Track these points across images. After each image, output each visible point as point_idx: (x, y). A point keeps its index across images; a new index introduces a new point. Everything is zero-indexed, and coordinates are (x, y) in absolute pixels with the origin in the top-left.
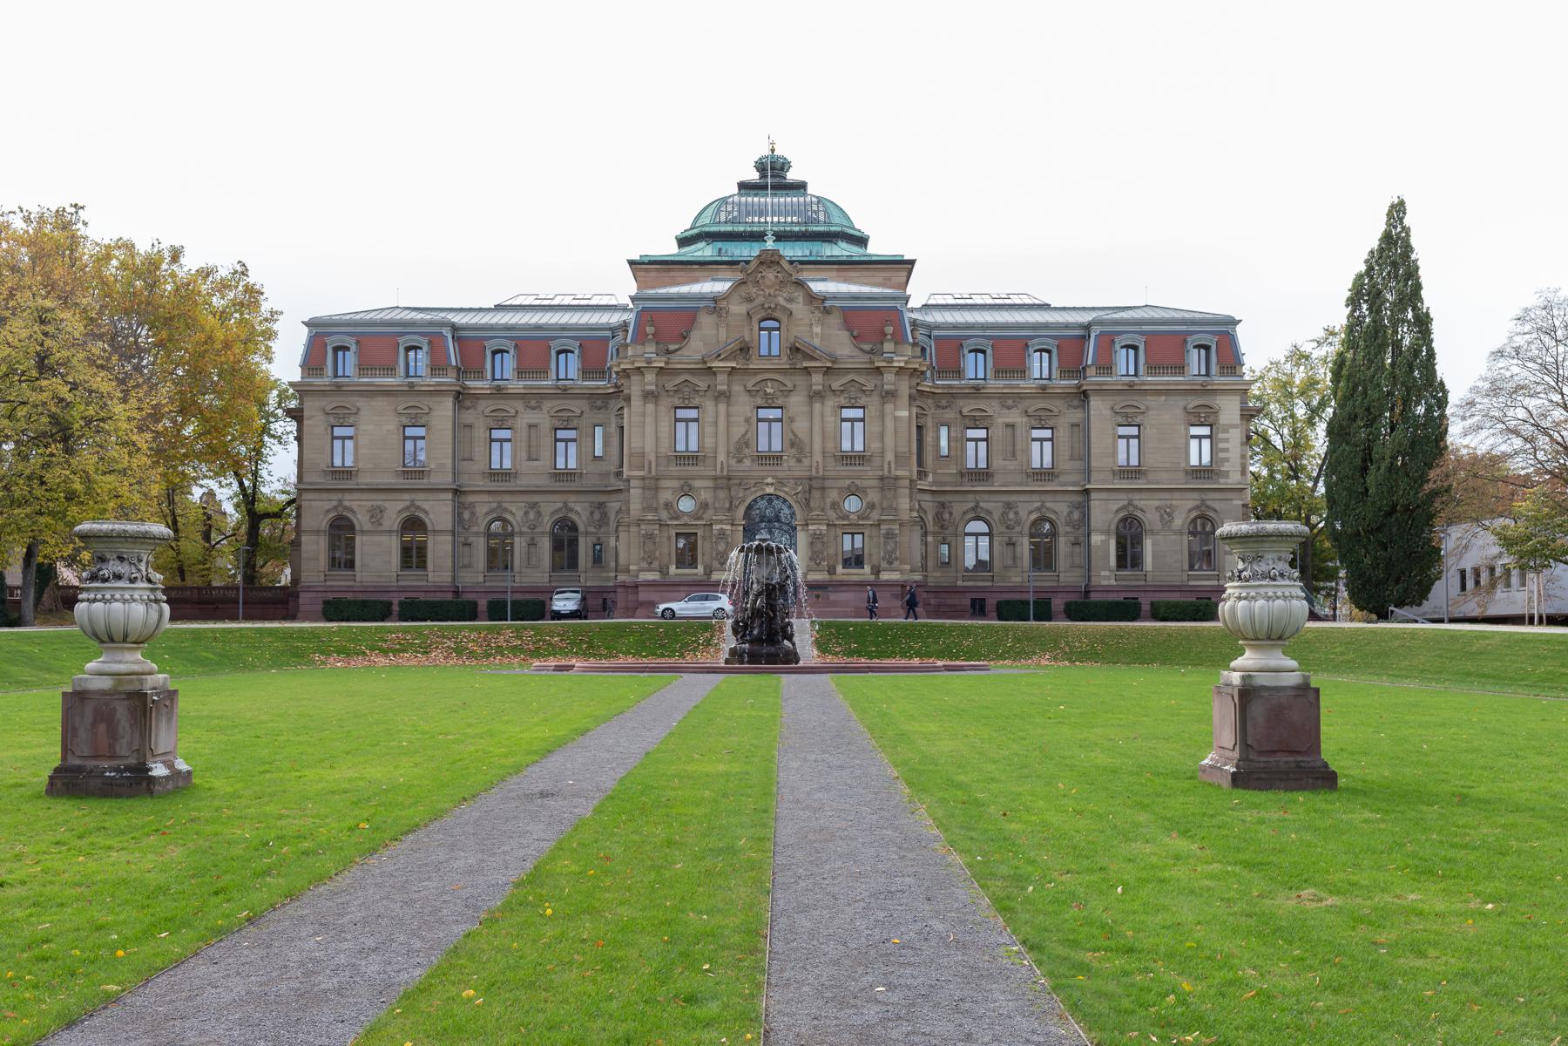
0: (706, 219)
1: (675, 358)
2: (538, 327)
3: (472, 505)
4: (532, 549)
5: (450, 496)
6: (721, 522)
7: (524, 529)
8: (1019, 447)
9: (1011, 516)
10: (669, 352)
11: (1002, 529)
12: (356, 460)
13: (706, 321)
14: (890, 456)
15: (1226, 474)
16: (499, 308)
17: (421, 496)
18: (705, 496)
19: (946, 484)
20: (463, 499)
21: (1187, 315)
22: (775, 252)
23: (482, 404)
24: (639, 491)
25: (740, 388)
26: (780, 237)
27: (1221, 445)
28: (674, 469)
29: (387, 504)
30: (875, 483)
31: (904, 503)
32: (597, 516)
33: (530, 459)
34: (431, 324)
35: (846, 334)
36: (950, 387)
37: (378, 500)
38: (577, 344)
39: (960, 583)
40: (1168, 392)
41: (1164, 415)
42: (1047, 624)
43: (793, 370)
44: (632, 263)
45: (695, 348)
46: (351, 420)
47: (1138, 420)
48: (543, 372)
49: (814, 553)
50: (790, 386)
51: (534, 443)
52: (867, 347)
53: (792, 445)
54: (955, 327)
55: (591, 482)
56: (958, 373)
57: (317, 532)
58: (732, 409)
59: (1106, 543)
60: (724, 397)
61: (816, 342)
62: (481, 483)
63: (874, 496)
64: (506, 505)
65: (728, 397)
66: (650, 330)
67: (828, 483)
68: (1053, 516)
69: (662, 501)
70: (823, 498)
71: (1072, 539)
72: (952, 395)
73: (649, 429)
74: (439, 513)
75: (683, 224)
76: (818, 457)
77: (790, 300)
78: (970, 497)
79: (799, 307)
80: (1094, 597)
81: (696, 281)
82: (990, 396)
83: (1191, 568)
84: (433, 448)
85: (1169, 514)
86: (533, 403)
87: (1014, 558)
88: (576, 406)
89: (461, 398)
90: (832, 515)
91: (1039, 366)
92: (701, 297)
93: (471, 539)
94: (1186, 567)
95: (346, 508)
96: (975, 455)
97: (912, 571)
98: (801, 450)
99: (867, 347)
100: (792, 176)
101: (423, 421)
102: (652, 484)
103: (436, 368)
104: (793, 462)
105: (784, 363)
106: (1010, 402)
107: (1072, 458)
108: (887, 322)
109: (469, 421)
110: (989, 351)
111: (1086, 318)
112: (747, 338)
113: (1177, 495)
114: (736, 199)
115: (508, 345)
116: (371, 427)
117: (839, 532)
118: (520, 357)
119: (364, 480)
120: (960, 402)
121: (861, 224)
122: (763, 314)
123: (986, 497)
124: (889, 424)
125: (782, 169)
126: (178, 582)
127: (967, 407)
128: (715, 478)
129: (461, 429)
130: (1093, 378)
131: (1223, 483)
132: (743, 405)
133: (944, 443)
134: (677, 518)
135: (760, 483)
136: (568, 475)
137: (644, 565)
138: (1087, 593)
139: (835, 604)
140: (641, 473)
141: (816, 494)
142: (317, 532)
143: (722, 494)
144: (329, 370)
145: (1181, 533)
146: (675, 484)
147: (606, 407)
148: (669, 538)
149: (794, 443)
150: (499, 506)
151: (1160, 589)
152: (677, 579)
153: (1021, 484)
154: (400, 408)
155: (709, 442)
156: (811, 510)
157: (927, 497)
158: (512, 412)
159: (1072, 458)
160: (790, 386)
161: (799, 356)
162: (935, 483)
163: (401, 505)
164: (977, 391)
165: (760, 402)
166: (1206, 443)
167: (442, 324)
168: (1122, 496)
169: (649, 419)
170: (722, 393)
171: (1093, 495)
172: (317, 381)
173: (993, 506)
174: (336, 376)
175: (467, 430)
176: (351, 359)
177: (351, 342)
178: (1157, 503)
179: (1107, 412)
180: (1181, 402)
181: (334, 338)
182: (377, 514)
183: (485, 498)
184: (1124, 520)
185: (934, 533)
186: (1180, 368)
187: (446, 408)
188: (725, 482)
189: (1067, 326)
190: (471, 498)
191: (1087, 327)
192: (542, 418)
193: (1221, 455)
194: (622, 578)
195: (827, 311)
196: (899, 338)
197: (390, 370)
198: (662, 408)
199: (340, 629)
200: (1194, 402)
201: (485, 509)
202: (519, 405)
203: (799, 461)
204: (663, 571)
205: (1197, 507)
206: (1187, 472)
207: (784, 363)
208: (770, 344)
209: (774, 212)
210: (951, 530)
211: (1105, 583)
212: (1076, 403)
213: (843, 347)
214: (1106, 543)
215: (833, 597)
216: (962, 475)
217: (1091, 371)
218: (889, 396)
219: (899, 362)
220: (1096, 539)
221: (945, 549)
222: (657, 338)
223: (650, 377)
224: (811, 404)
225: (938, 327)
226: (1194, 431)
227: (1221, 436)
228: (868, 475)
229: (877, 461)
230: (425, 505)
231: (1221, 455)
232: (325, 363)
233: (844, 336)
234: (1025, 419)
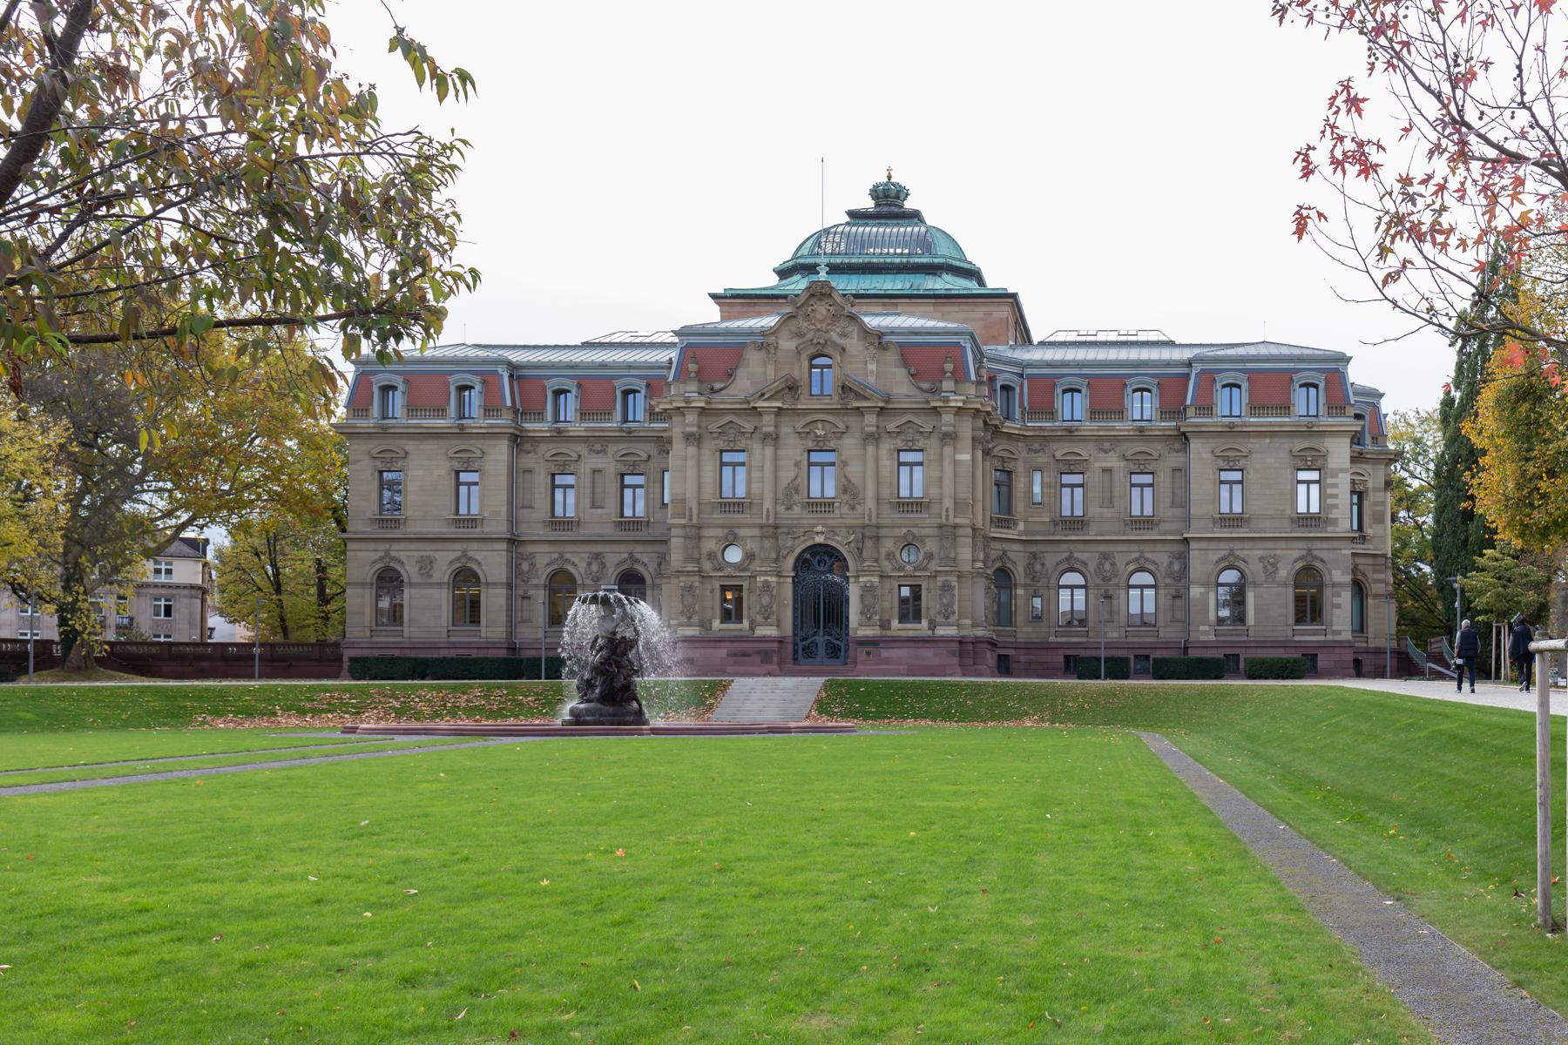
1: (717, 397)
2: (603, 365)
3: (531, 556)
5: (504, 546)
6: (765, 573)
7: (588, 582)
9: (1107, 566)
10: (713, 391)
11: (1099, 581)
12: (482, 505)
13: (753, 357)
14: (948, 503)
15: (1335, 522)
16: (587, 345)
17: (474, 546)
18: (752, 545)
19: (1038, 533)
21: (1285, 351)
22: (826, 283)
23: (543, 447)
26: (834, 269)
27: (1329, 491)
28: (718, 517)
29: (437, 555)
31: (965, 553)
33: (593, 506)
34: (485, 361)
35: (903, 371)
36: (1041, 428)
37: (427, 550)
38: (643, 383)
39: (1052, 639)
40: (1272, 434)
41: (1268, 458)
42: (1126, 682)
43: (844, 411)
44: (714, 296)
45: (742, 386)
46: (399, 465)
47: (1241, 464)
48: (607, 414)
49: (865, 606)
51: (598, 490)
52: (926, 386)
53: (845, 491)
54: (1049, 364)
56: (1051, 414)
57: (363, 585)
58: (780, 453)
59: (1205, 596)
60: (774, 439)
61: (871, 380)
62: (541, 532)
63: (932, 546)
66: (692, 367)
67: (883, 532)
68: (1152, 568)
70: (877, 548)
71: (1173, 591)
72: (1045, 438)
73: (691, 473)
74: (492, 563)
75: (784, 255)
76: (871, 503)
77: (844, 335)
78: (1064, 547)
79: (854, 344)
80: (1194, 654)
81: (759, 314)
82: (1085, 439)
83: (1298, 621)
84: (485, 496)
87: (1111, 612)
89: (518, 440)
90: (887, 566)
91: (1142, 407)
92: (750, 333)
93: (531, 592)
94: (1291, 620)
95: (393, 558)
96: (1071, 503)
98: (855, 496)
99: (926, 386)
100: (909, 204)
101: (476, 466)
102: (695, 534)
103: (490, 409)
104: (845, 510)
105: (835, 403)
106: (1107, 445)
108: (946, 359)
110: (1322, 386)
111: (1187, 354)
112: (797, 376)
113: (1282, 544)
115: (571, 385)
116: (420, 473)
118: (409, 394)
119: (414, 528)
120: (1053, 445)
121: (974, 255)
122: (813, 350)
123: (1081, 547)
125: (898, 197)
126: (279, 638)
128: (762, 526)
129: (517, 476)
130: (1193, 420)
131: (1331, 531)
133: (1037, 489)
134: (721, 570)
135: (809, 532)
136: (636, 524)
138: (1186, 648)
139: (887, 661)
140: (683, 521)
141: (869, 544)
142: (363, 585)
143: (767, 544)
144: (375, 410)
145: (1285, 585)
146: (719, 532)
148: (712, 591)
149: (847, 488)
151: (1262, 645)
152: (720, 634)
153: (1118, 533)
155: (755, 487)
156: (864, 560)
157: (1017, 547)
158: (575, 456)
160: (842, 427)
161: (852, 395)
162: (1025, 532)
163: (452, 556)
164: (1070, 434)
165: (811, 445)
166: (1315, 489)
167: (497, 362)
168: (1223, 545)
170: (767, 436)
171: (1193, 545)
172: (363, 424)
173: (1089, 556)
174: (557, 421)
175: (527, 475)
176: (398, 400)
177: (571, 385)
178: (1261, 553)
179: (1207, 456)
180: (1287, 444)
181: (380, 376)
182: (426, 565)
183: (546, 548)
184: (1305, 568)
185: (1025, 586)
186: (1286, 408)
187: (499, 454)
188: (773, 530)
189: (1168, 364)
190: (530, 549)
191: (1189, 364)
192: (608, 463)
193: (1329, 501)
195: (882, 347)
196: (959, 376)
197: (441, 411)
199: (261, 687)
200: (1299, 444)
201: (546, 561)
202: (582, 449)
203: (853, 508)
204: (885, 625)
205: (1303, 558)
206: (1292, 520)
207: (835, 403)
208: (825, 382)
209: (889, 241)
210: (1043, 582)
212: (1177, 446)
213: (900, 386)
214: (1205, 596)
215: (885, 653)
216: (1055, 523)
217: (1191, 412)
218: (950, 438)
219: (956, 401)
220: (1195, 591)
221: (1037, 602)
222: (700, 376)
223: (691, 418)
225: (1031, 364)
226: (1302, 475)
227: (1329, 481)
228: (925, 524)
229: (935, 509)
230: (479, 556)
231: (1329, 501)
232: (545, 408)
233: (901, 374)
234: (1123, 464)
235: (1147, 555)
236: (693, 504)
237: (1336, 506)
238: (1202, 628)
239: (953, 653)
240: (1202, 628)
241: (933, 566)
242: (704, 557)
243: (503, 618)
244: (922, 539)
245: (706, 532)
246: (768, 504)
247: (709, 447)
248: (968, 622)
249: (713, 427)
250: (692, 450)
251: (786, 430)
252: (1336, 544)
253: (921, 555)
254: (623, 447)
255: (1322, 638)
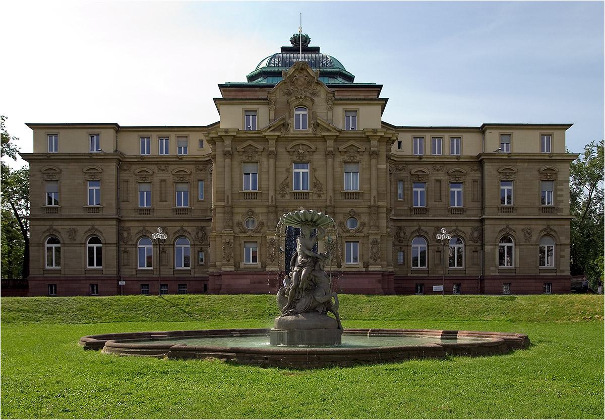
0: (264, 64)
4: (163, 255)
5: (114, 222)
8: (443, 193)
14: (374, 193)
17: (98, 222)
18: (262, 218)
20: (122, 225)
24: (221, 215)
25: (284, 150)
27: (559, 193)
29: (78, 228)
30: (366, 210)
32: (200, 235)
39: (409, 274)
44: (220, 86)
46: (57, 177)
50: (313, 148)
55: (197, 214)
58: (277, 163)
59: (493, 250)
60: (274, 155)
63: (365, 218)
64: (147, 228)
65: (276, 155)
67: (337, 210)
69: (235, 222)
74: (109, 232)
76: (330, 193)
78: (415, 223)
82: (427, 163)
85: (529, 234)
86: (163, 167)
88: (189, 168)
95: (55, 230)
97: (388, 266)
98: (320, 189)
104: (315, 197)
106: (438, 167)
107: (473, 201)
109: (126, 178)
113: (534, 222)
114: (281, 55)
117: (344, 241)
119: (65, 213)
120: (410, 167)
121: (349, 69)
123: (425, 223)
124: (374, 172)
127: (414, 169)
128: (268, 207)
132: (285, 160)
134: (245, 233)
137: (225, 262)
140: (223, 204)
147: (205, 170)
150: (144, 229)
153: (445, 216)
154: (85, 169)
159: (473, 201)
165: (295, 158)
168: (503, 222)
169: (227, 169)
170: (272, 152)
171: (487, 222)
178: (522, 227)
179: (495, 173)
180: (537, 166)
182: (73, 233)
183: (136, 224)
190: (128, 224)
192: (168, 177)
193: (559, 199)
194: (211, 270)
198: (235, 163)
201: (136, 231)
203: (319, 196)
205: (545, 229)
211: (493, 274)
212: (476, 168)
214: (493, 250)
220: (488, 248)
223: (228, 142)
224: (326, 159)
229: (366, 197)
231: (559, 199)
234: (447, 177)
235: (460, 228)
236: (228, 193)
237: (562, 201)
238: (491, 269)
239: (379, 281)
240: (491, 269)
241: (365, 230)
242: (235, 225)
243: (115, 263)
244: (359, 215)
245: (236, 210)
246: (271, 193)
247: (238, 158)
248: (385, 263)
249: (240, 148)
250: (228, 161)
251: (281, 150)
252: (562, 222)
253: (359, 224)
254: (177, 168)
255: (555, 274)
